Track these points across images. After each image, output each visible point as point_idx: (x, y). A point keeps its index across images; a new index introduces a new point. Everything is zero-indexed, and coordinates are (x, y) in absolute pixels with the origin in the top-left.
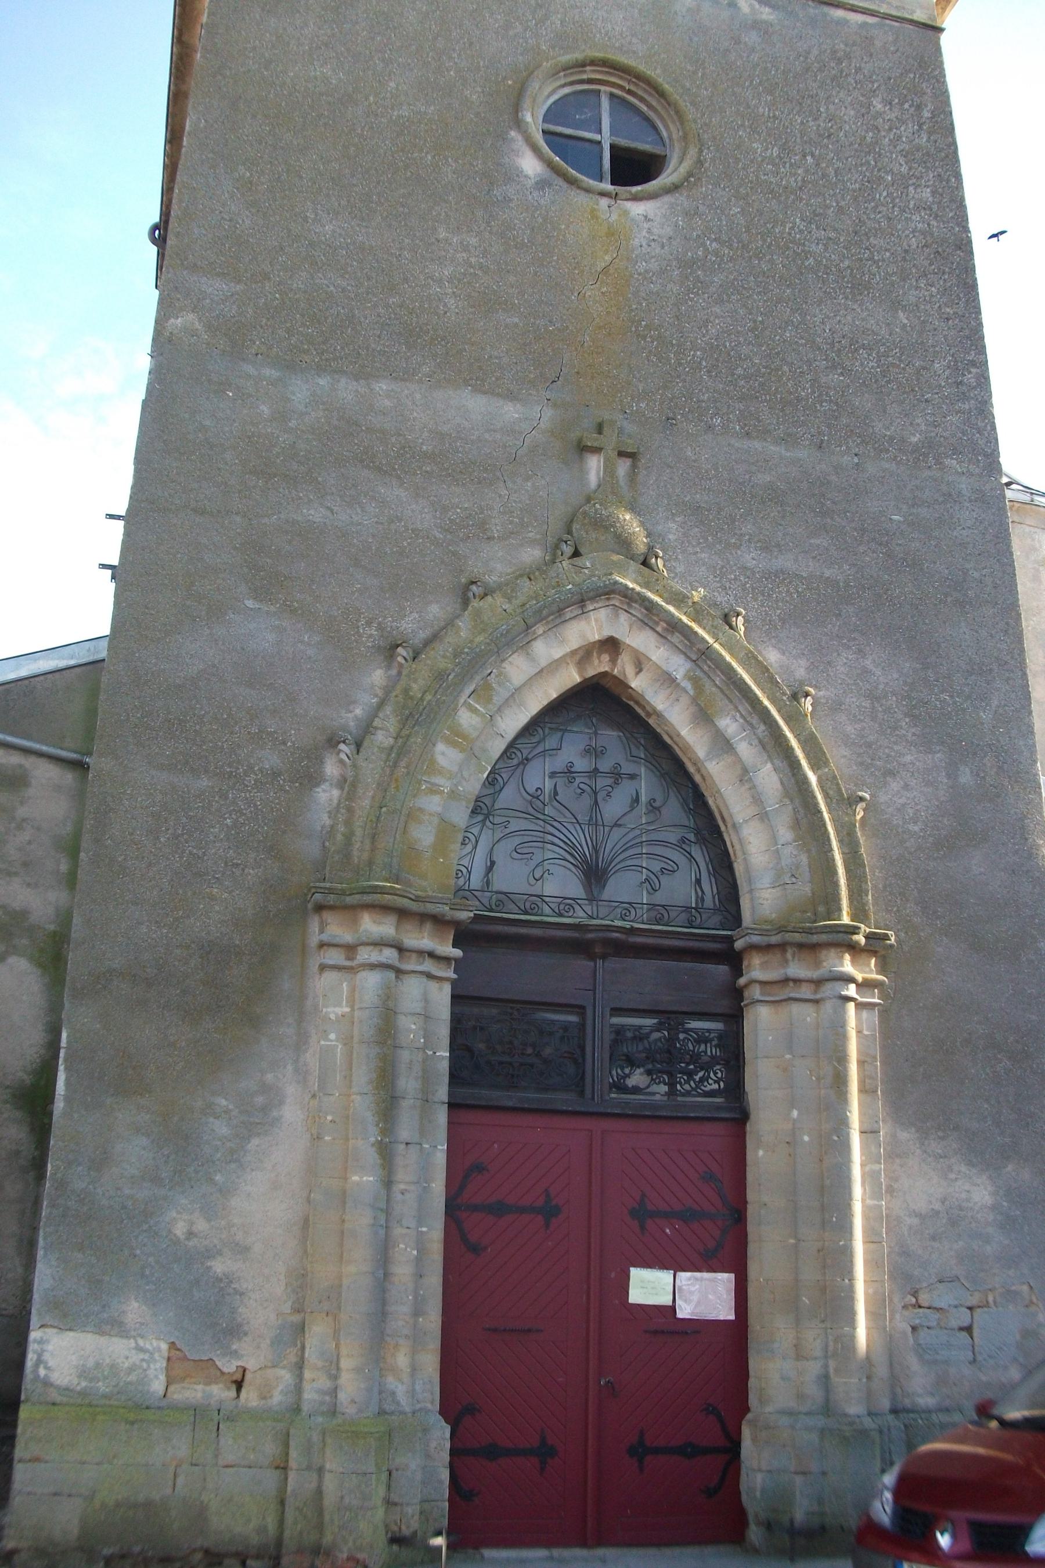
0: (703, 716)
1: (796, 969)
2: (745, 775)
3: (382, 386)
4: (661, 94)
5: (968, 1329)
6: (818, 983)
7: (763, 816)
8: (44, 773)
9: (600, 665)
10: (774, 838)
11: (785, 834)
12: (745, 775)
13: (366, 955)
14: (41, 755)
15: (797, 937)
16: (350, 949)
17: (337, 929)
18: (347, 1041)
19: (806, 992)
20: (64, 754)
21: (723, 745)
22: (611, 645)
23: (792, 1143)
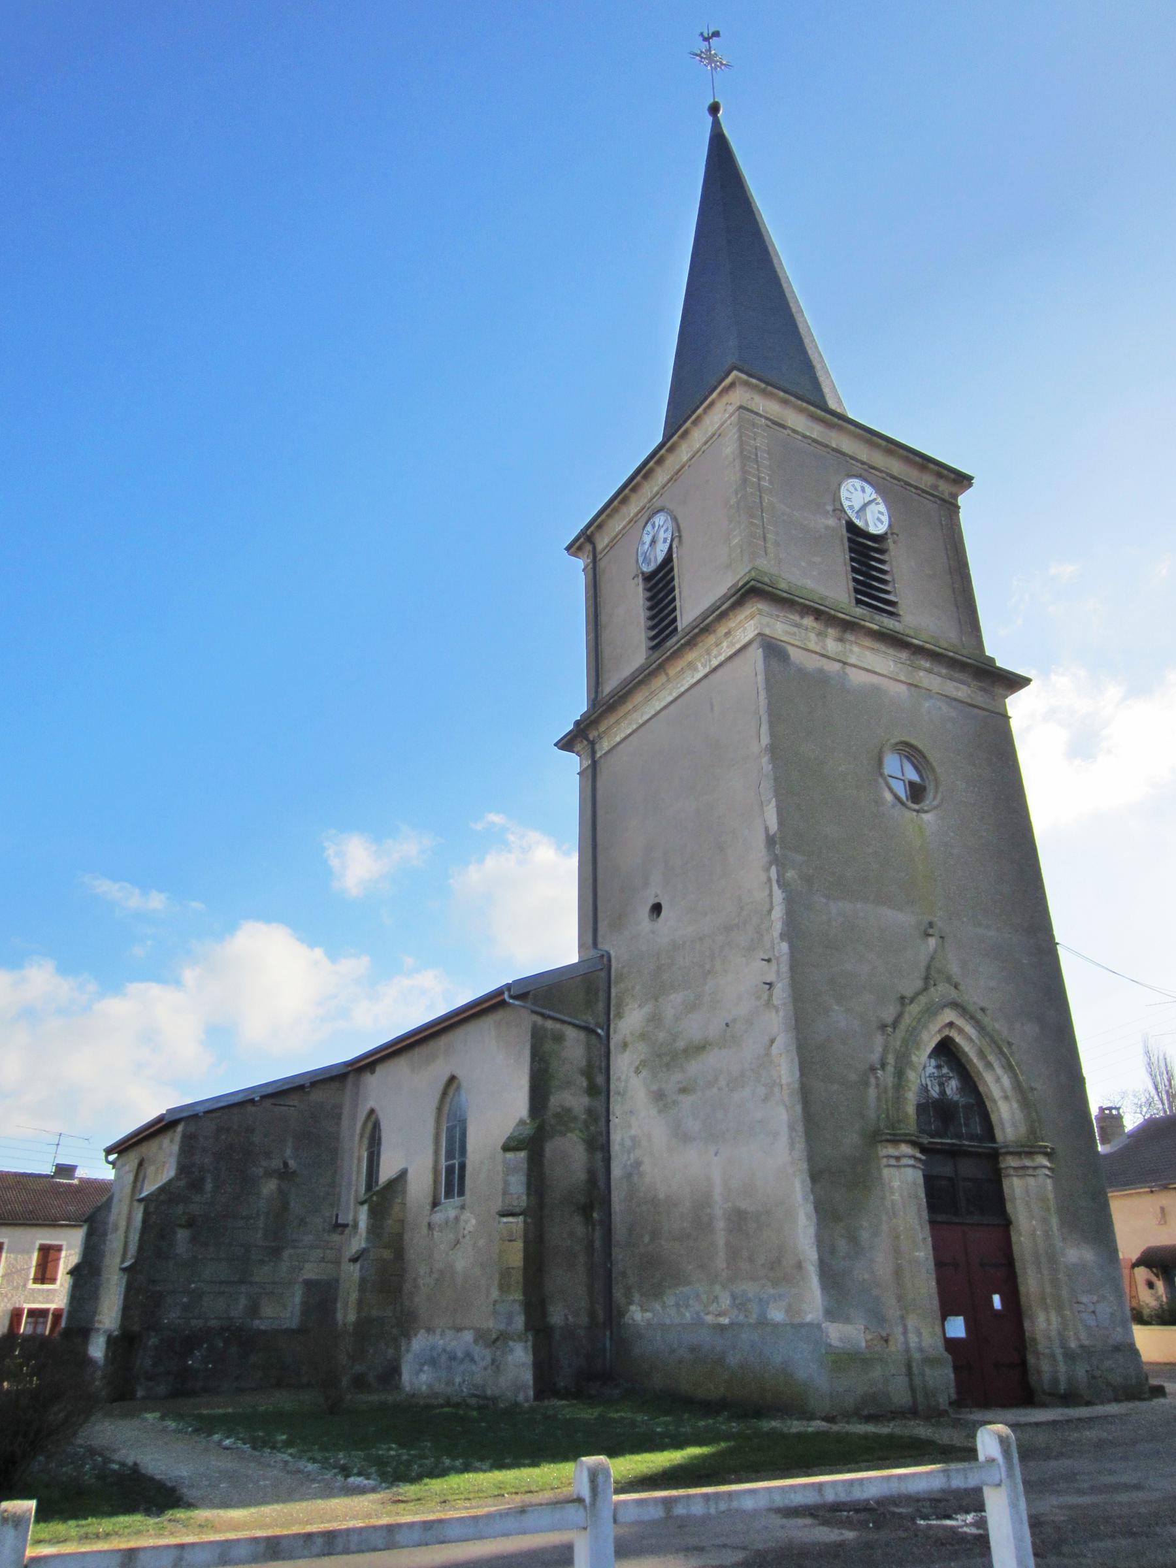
0: (982, 1054)
1: (1027, 1162)
2: (998, 1080)
3: (859, 906)
4: (924, 757)
5: (1094, 1312)
6: (1035, 1168)
7: (1006, 1098)
8: (571, 1033)
9: (946, 1032)
10: (1011, 1108)
11: (1015, 1105)
12: (998, 1080)
13: (905, 1161)
14: (570, 1023)
15: (1027, 1149)
16: (898, 1158)
17: (891, 1150)
18: (901, 1196)
19: (1030, 1172)
20: (577, 1022)
21: (989, 1065)
22: (951, 1025)
23: (1033, 1234)
